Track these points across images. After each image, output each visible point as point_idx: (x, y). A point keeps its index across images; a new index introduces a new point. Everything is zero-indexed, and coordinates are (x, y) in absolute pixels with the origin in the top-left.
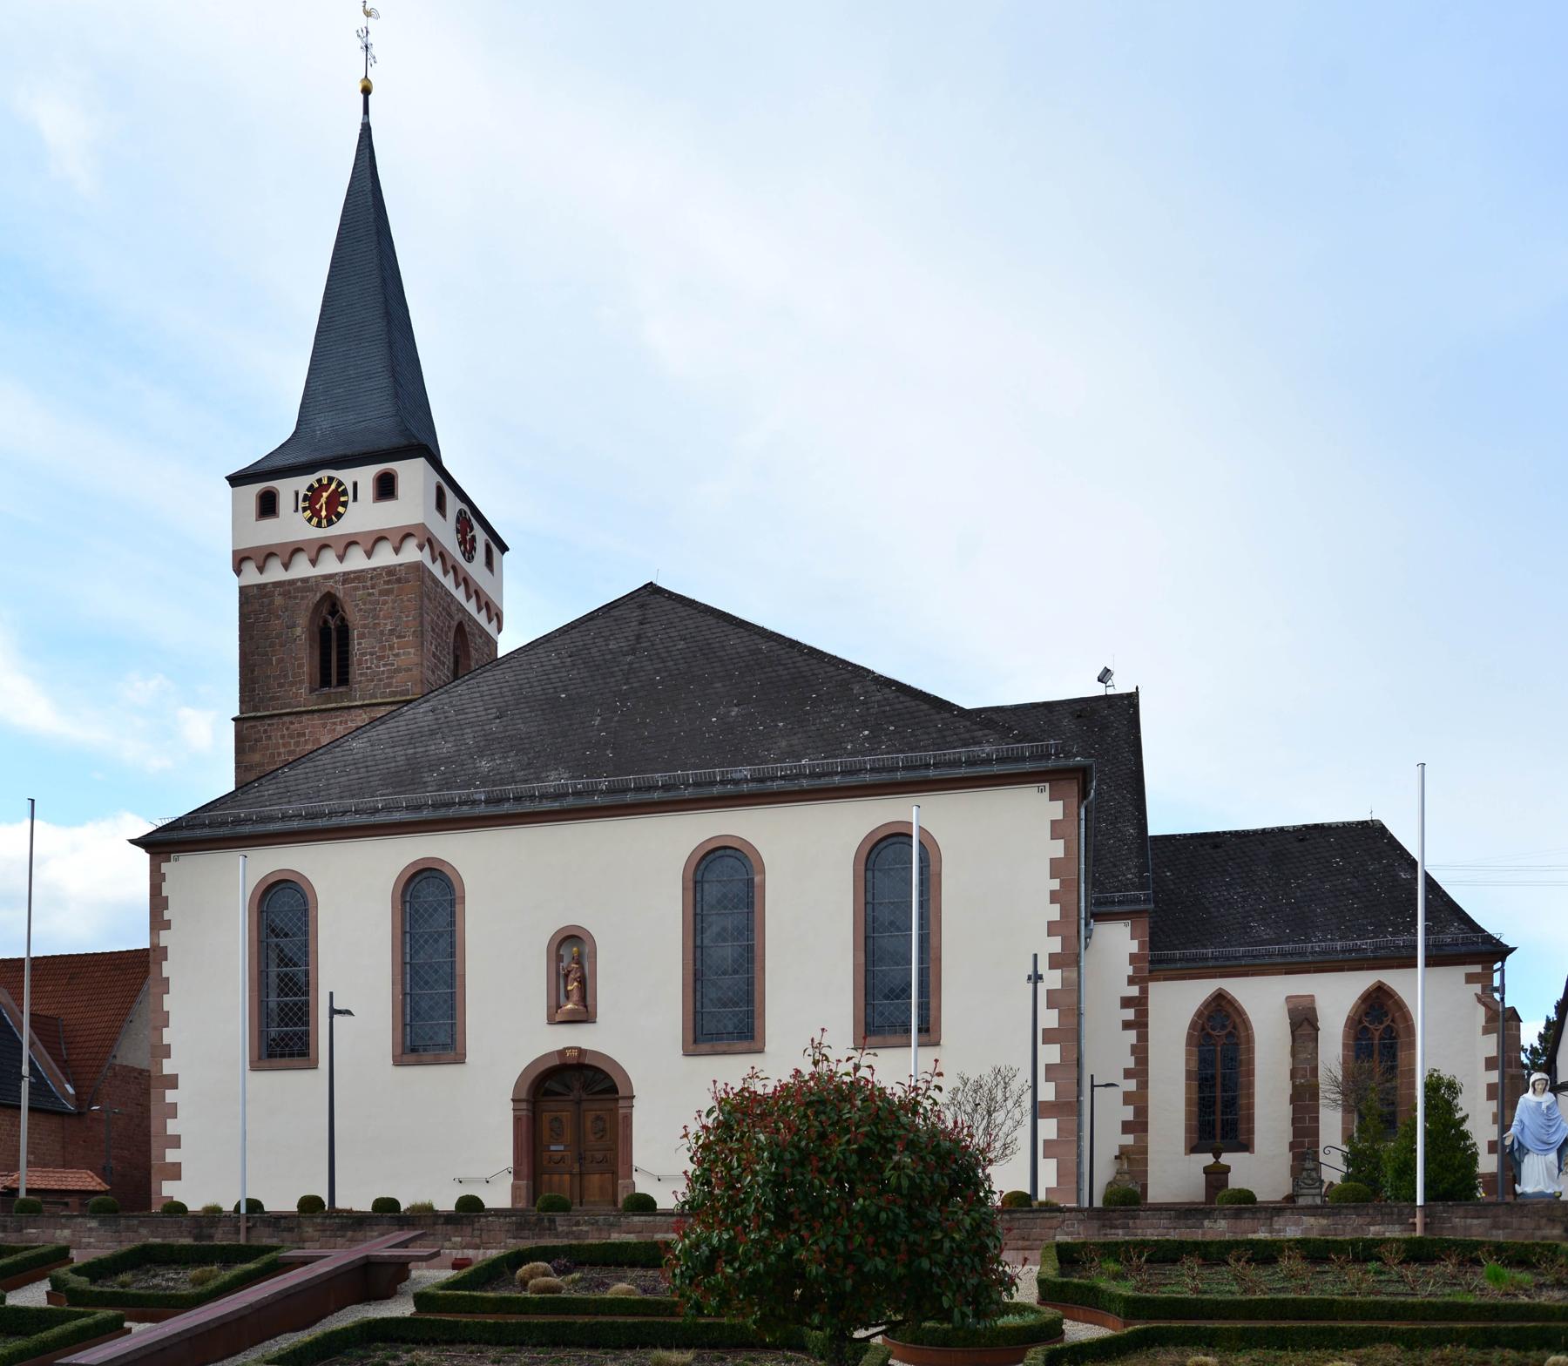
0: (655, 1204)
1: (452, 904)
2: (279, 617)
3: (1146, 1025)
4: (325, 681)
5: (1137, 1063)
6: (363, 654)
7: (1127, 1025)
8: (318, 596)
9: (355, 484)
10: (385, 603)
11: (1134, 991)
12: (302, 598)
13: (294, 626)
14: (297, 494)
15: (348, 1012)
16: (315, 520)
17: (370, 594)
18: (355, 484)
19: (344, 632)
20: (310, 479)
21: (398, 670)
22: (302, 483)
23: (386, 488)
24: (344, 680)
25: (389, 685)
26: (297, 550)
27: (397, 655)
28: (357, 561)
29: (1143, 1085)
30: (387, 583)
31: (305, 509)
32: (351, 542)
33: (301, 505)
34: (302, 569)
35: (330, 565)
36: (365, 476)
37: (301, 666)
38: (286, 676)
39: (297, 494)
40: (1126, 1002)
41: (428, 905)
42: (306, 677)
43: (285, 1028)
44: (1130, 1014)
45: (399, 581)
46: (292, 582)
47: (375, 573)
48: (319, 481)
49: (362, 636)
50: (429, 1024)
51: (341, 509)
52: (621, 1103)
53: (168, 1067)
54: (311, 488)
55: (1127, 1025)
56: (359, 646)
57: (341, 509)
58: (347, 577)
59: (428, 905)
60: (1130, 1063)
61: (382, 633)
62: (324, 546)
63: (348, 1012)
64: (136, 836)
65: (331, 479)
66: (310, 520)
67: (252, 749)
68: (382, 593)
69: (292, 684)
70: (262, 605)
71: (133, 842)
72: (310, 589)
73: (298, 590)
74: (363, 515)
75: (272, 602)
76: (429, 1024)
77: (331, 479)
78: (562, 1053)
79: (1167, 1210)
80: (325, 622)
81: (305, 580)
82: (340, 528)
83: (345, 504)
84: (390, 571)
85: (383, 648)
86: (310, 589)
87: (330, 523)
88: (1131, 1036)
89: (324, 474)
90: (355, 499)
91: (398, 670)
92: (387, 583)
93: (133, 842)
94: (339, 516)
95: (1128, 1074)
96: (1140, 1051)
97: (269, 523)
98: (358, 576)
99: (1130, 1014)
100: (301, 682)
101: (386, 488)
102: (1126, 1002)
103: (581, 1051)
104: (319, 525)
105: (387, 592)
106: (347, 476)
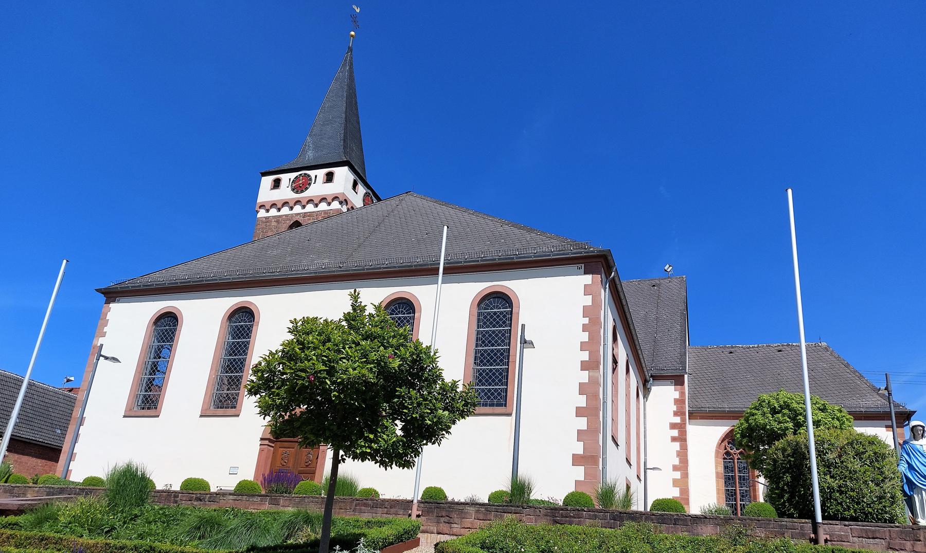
3: (685, 440)
5: (680, 462)
7: (674, 439)
11: (677, 420)
15: (115, 360)
22: (293, 175)
26: (285, 203)
28: (310, 208)
29: (685, 475)
32: (310, 201)
36: (321, 173)
40: (673, 426)
44: (675, 433)
46: (280, 216)
55: (674, 439)
58: (305, 215)
60: (676, 461)
62: (298, 202)
63: (115, 360)
64: (103, 286)
71: (97, 290)
74: (319, 188)
81: (286, 216)
82: (308, 193)
84: (325, 212)
88: (677, 446)
93: (97, 290)
95: (675, 468)
96: (683, 455)
98: (310, 214)
99: (675, 433)
101: (330, 178)
102: (673, 426)
106: (312, 173)
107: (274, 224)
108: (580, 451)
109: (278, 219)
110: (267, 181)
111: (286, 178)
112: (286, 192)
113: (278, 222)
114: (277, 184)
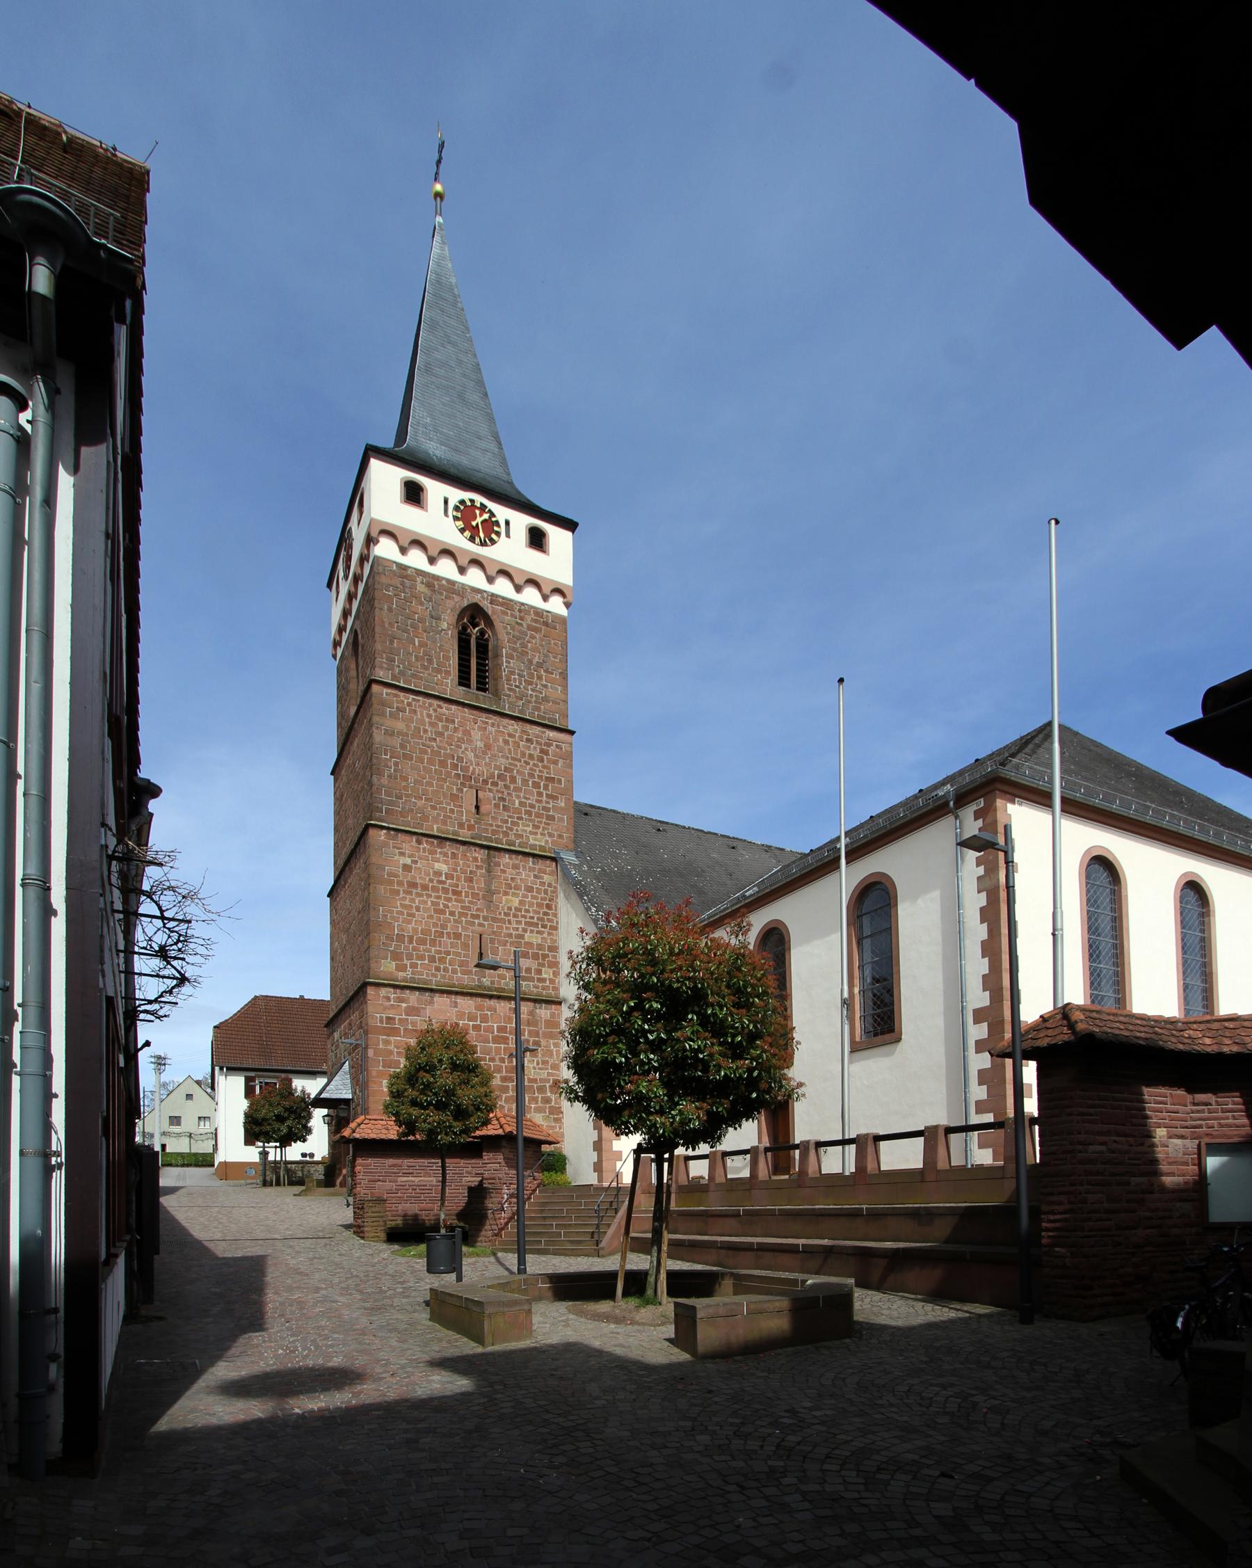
2: (422, 604)
4: (464, 680)
6: (512, 673)
8: (466, 603)
10: (533, 637)
16: (467, 534)
18: (507, 523)
20: (467, 496)
21: (546, 699)
22: (456, 495)
26: (448, 552)
27: (546, 686)
28: (503, 588)
35: (474, 578)
36: (521, 522)
37: (447, 658)
38: (430, 661)
49: (510, 657)
57: (494, 536)
61: (530, 662)
62: (476, 562)
68: (530, 628)
69: (438, 671)
70: (403, 584)
75: (413, 587)
83: (498, 534)
87: (483, 544)
89: (479, 499)
91: (546, 699)
92: (536, 621)
94: (493, 542)
100: (448, 673)
104: (472, 539)
105: (537, 630)
106: (502, 512)
107: (421, 588)
111: (435, 490)
113: (429, 585)
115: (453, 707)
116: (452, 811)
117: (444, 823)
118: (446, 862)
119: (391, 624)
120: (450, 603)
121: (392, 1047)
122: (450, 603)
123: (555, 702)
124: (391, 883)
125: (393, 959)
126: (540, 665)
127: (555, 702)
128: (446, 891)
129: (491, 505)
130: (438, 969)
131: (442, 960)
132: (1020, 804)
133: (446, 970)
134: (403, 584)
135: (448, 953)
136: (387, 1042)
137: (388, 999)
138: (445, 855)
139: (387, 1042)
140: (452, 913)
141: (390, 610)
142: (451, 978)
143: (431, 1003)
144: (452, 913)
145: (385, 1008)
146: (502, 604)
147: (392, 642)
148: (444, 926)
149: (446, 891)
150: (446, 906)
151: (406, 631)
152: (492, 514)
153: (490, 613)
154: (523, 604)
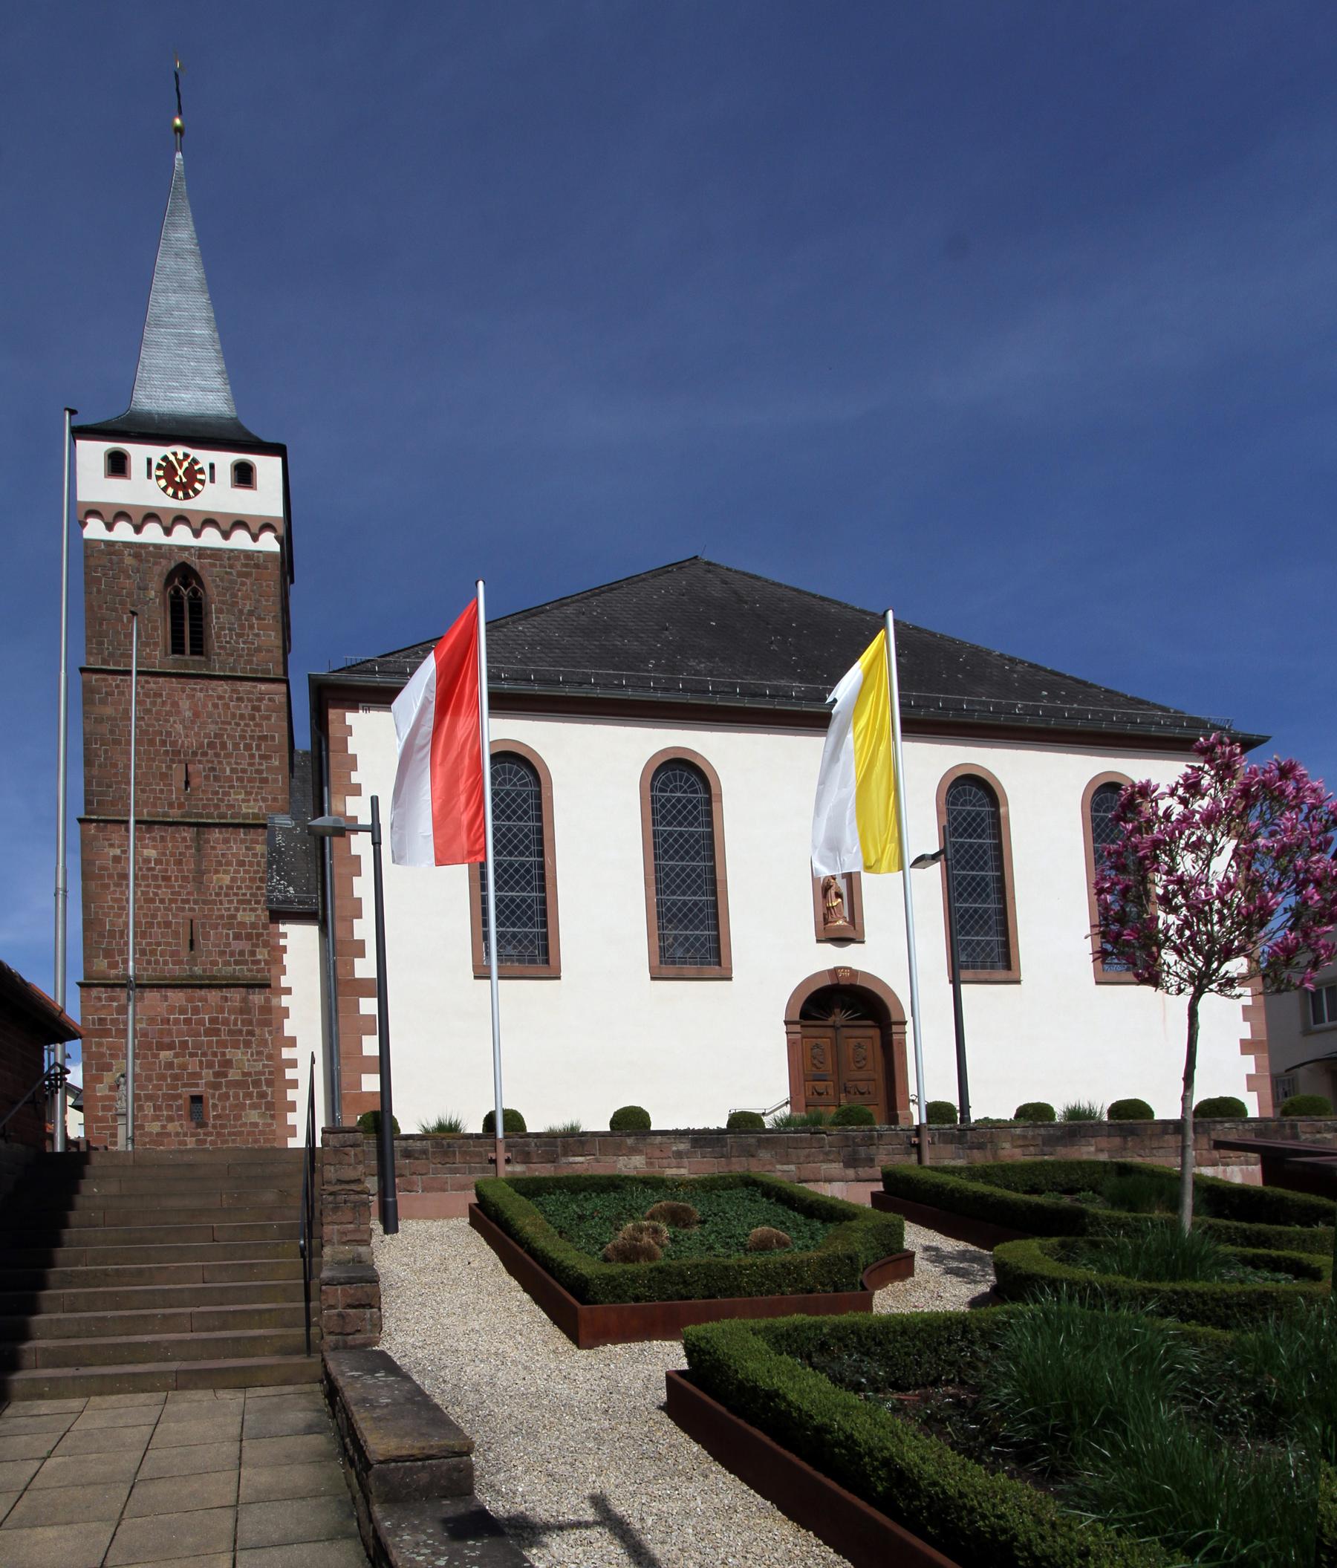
0: (1150, 1113)
1: (709, 802)
2: (129, 577)
4: (177, 648)
6: (223, 629)
8: (173, 565)
9: (212, 466)
10: (243, 584)
12: (156, 564)
13: (146, 589)
14: (149, 462)
17: (227, 573)
18: (212, 466)
19: (198, 609)
20: (167, 451)
21: (258, 650)
22: (157, 452)
23: (244, 476)
24: (199, 647)
25: (250, 662)
26: (151, 516)
27: (257, 635)
28: (211, 538)
30: (246, 566)
31: (158, 478)
32: (210, 521)
33: (155, 472)
34: (152, 534)
35: (182, 536)
36: (225, 461)
37: (155, 629)
39: (149, 462)
41: (681, 804)
42: (160, 640)
43: (982, 937)
45: (257, 566)
47: (234, 554)
48: (175, 454)
49: (220, 611)
50: (689, 930)
51: (197, 486)
52: (895, 1028)
53: (285, 981)
54: (165, 458)
56: (217, 621)
57: (197, 486)
58: (202, 552)
59: (681, 804)
61: (241, 612)
62: (181, 518)
65: (186, 456)
66: (165, 489)
67: (103, 702)
68: (240, 574)
70: (111, 561)
72: (162, 556)
73: (149, 553)
75: (121, 561)
76: (689, 930)
77: (186, 456)
78: (835, 971)
79: (728, 1187)
80: (177, 590)
81: (158, 547)
83: (202, 482)
84: (248, 555)
85: (242, 627)
86: (162, 556)
87: (187, 497)
89: (181, 450)
90: (212, 480)
92: (246, 566)
94: (197, 492)
97: (117, 482)
98: (216, 553)
100: (156, 644)
101: (244, 476)
103: (854, 973)
105: (247, 575)
106: (205, 457)
107: (129, 561)
108: (1248, 1036)
109: (138, 550)
110: (92, 453)
111: (138, 453)
112: (142, 489)
113: (137, 556)
114: (117, 465)
115: (161, 680)
116: (162, 791)
117: (155, 805)
118: (154, 847)
119: (100, 607)
120: (157, 569)
121: (104, 1049)
122: (157, 569)
123: (268, 651)
124: (102, 877)
125: (105, 957)
126: (251, 613)
127: (268, 651)
128: (155, 878)
129: (194, 453)
130: (149, 962)
131: (153, 952)
132: (367, 709)
133: (157, 962)
134: (111, 561)
135: (158, 944)
136: (99, 1045)
137: (99, 999)
138: (154, 839)
139: (99, 1045)
140: (162, 901)
141: (99, 591)
142: (162, 971)
143: (142, 998)
144: (162, 901)
145: (97, 1010)
146: (210, 557)
147: (101, 625)
148: (154, 916)
149: (155, 878)
150: (156, 894)
151: (115, 610)
152: (195, 461)
153: (197, 568)
154: (232, 550)
